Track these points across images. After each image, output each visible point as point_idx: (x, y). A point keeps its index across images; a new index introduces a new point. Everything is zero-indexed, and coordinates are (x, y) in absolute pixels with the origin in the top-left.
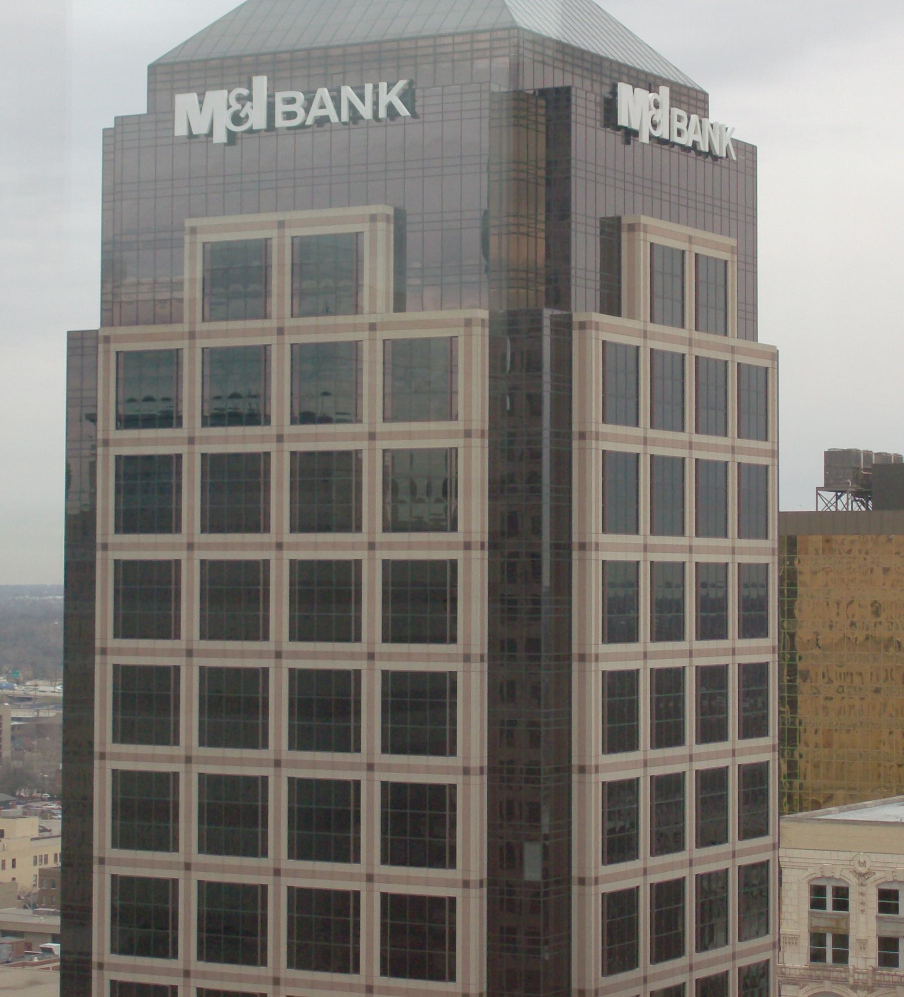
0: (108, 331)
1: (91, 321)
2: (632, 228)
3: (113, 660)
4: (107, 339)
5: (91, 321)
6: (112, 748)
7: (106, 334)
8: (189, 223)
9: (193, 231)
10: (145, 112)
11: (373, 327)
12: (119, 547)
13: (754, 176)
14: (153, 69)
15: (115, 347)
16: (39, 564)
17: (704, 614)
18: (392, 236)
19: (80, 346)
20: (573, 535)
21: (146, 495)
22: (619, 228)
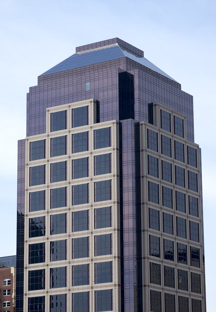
0: (28, 138)
1: (24, 136)
2: (155, 105)
3: (28, 296)
4: (28, 140)
5: (24, 136)
6: (28, 292)
7: (27, 138)
8: (47, 109)
9: (48, 111)
10: (37, 85)
11: (91, 127)
12: (30, 241)
13: (192, 103)
14: (39, 78)
15: (29, 141)
16: (9, 249)
17: (180, 256)
18: (120, 290)
19: (21, 143)
20: (141, 201)
21: (37, 175)
22: (152, 105)
